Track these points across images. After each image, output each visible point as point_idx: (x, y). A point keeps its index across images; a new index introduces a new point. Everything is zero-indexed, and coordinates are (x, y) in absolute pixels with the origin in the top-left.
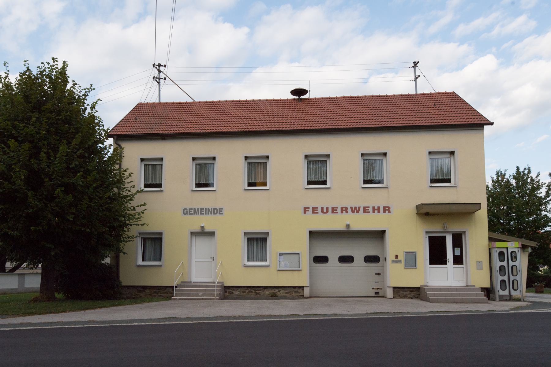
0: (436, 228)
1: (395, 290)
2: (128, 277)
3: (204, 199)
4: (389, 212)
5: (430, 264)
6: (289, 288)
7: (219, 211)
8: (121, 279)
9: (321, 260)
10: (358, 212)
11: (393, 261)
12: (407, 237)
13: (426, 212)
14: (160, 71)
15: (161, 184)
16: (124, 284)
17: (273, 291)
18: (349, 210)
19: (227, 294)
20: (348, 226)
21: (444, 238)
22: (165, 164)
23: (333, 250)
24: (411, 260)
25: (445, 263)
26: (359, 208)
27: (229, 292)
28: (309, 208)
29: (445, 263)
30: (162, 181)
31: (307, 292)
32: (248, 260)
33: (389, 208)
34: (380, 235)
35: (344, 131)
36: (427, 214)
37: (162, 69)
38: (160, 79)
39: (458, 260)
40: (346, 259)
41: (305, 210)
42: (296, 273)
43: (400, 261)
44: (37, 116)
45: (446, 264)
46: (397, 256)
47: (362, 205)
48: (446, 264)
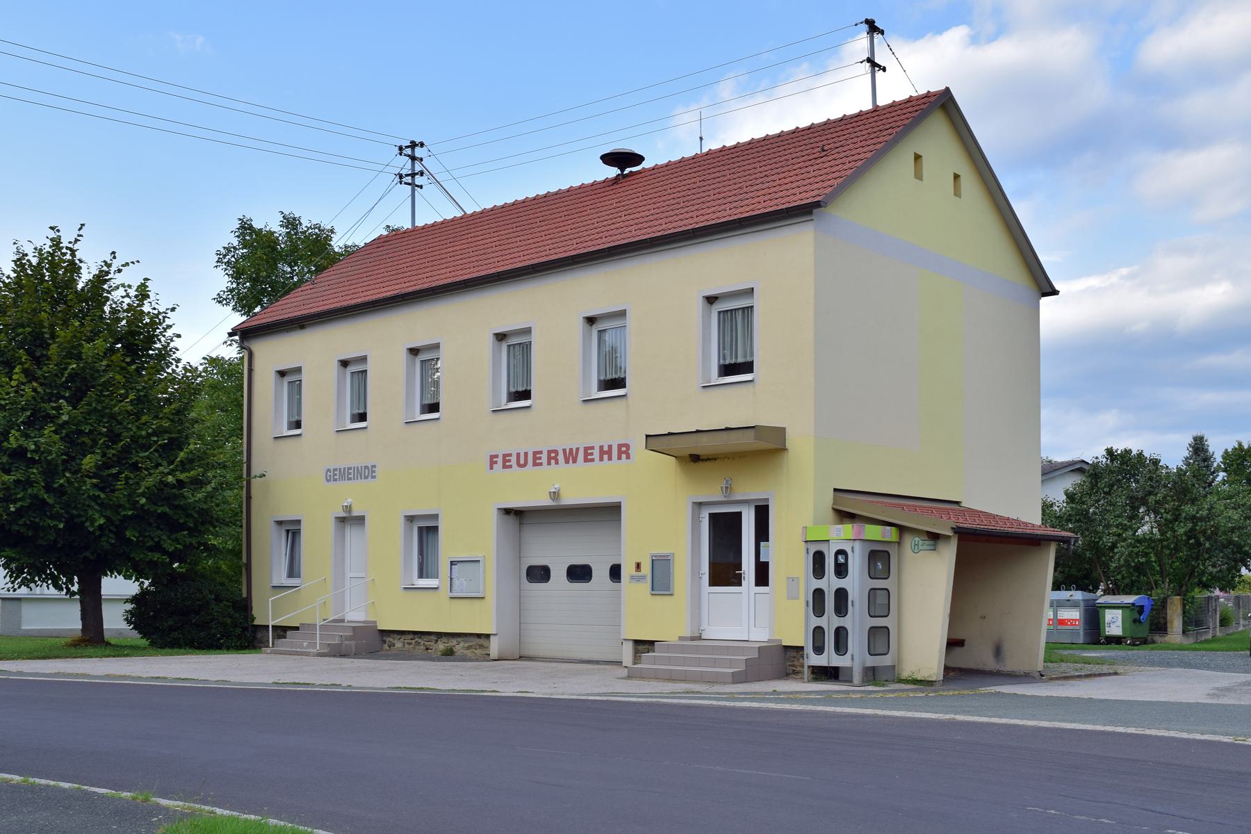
0: (711, 491)
1: (640, 647)
2: (266, 612)
3: (356, 450)
4: (628, 457)
5: (757, 585)
6: (472, 639)
7: (368, 472)
8: (255, 612)
9: (540, 574)
10: (575, 461)
11: (632, 578)
12: (663, 517)
13: (696, 454)
14: (413, 158)
15: (751, 363)
16: (256, 622)
17: (450, 644)
18: (561, 457)
19: (386, 646)
20: (555, 495)
21: (738, 515)
22: (760, 303)
23: (557, 551)
24: (660, 576)
25: (738, 582)
26: (578, 449)
27: (380, 642)
28: (592, 448)
29: (738, 582)
30: (752, 354)
31: (494, 647)
32: (421, 576)
33: (627, 446)
34: (610, 512)
35: (467, 287)
36: (695, 458)
37: (419, 152)
38: (413, 175)
39: (762, 577)
40: (579, 573)
41: (493, 460)
42: (476, 602)
43: (644, 577)
44: (87, 346)
45: (740, 584)
46: (638, 566)
47: (579, 443)
48: (740, 584)
